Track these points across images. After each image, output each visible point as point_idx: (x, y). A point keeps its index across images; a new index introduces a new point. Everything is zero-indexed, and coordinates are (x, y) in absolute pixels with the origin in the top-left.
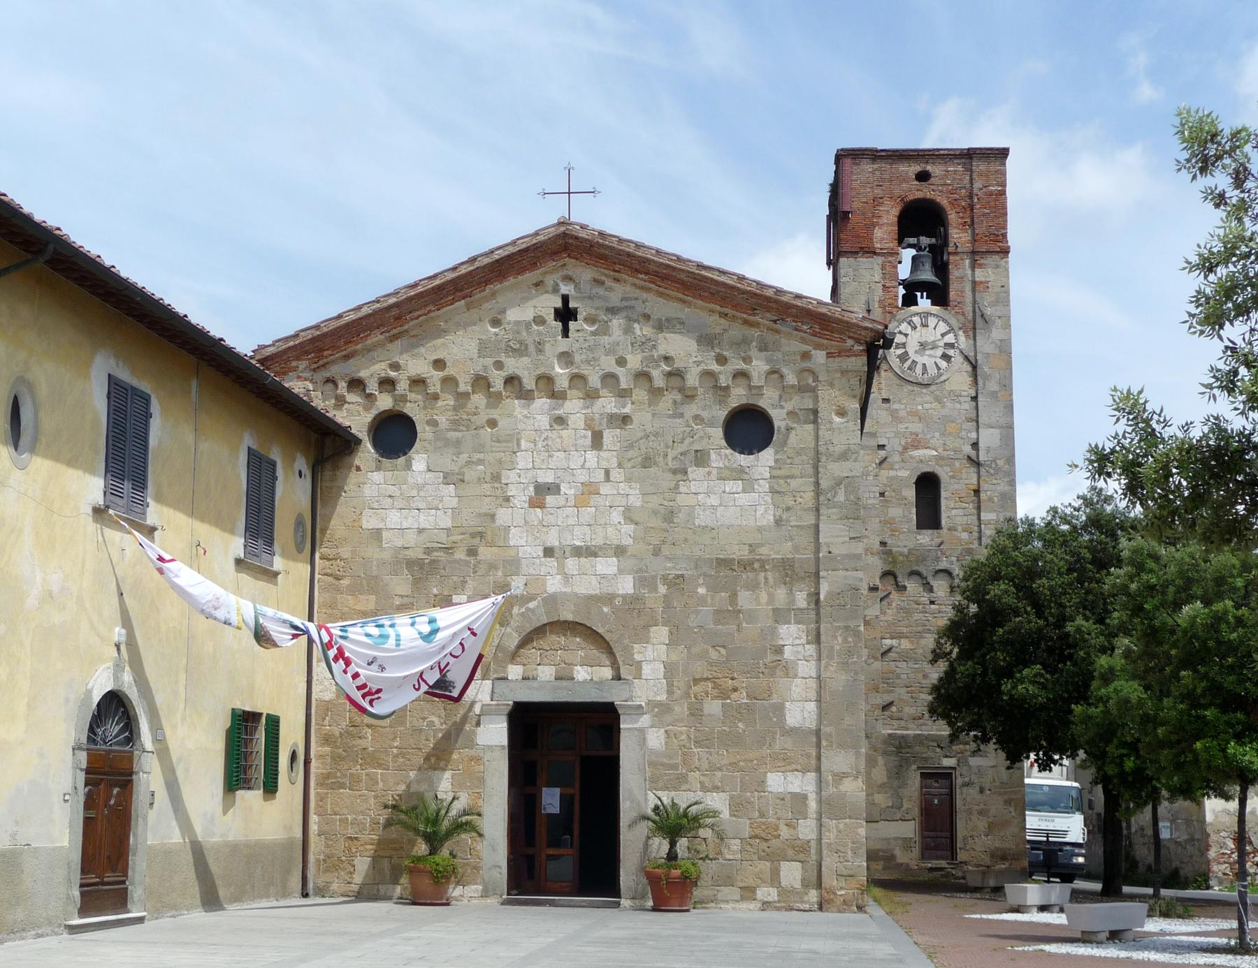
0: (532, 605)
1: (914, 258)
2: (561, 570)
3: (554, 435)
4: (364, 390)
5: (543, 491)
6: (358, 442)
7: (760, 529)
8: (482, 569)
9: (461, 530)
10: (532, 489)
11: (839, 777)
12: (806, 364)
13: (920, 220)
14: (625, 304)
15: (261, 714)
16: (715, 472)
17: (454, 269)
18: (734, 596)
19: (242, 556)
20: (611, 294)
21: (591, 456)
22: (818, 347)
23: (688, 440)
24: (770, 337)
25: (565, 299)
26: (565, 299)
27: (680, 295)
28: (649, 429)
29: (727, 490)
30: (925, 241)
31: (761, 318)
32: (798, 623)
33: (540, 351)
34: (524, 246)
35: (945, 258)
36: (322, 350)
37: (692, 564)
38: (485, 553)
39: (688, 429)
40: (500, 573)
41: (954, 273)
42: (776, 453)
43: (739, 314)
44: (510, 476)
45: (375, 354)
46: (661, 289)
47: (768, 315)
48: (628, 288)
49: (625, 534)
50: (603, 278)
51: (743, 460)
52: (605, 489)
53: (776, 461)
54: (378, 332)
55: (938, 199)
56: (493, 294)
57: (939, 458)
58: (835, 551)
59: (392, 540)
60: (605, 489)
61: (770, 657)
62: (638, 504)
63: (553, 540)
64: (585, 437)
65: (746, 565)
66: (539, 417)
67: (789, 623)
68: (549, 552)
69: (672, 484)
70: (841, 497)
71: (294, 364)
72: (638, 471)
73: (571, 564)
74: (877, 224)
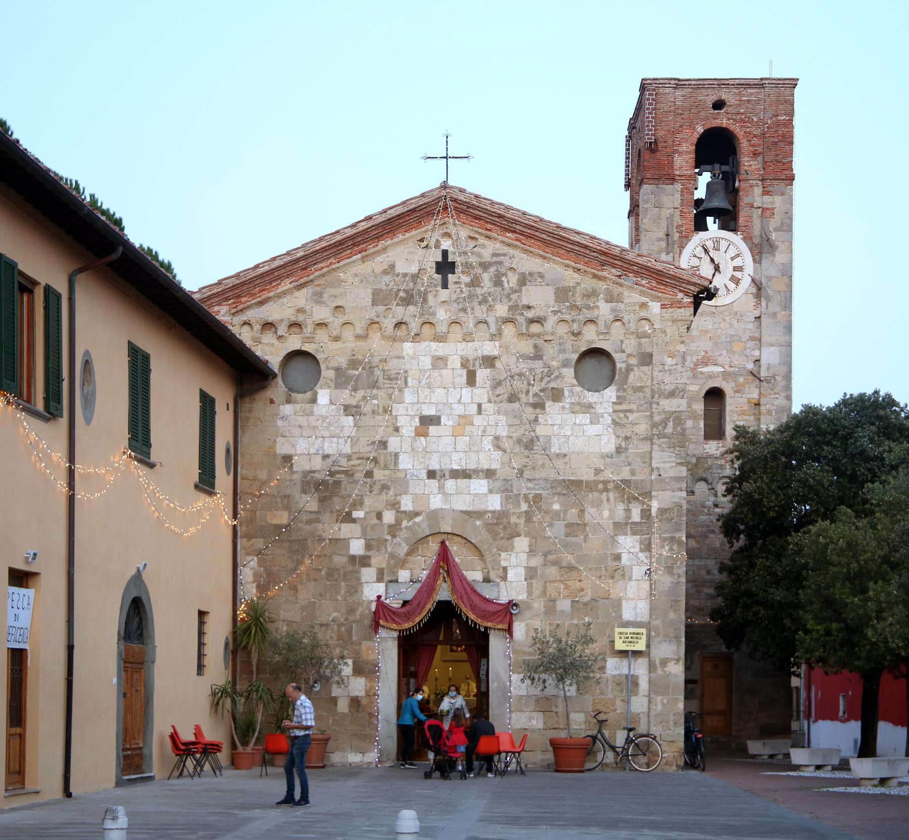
0: (418, 519)
5: (428, 421)
11: (664, 662)
13: (716, 149)
21: (466, 392)
22: (658, 299)
43: (589, 269)
44: (398, 409)
49: (491, 459)
53: (618, 397)
58: (664, 475)
59: (301, 465)
60: (478, 420)
61: (612, 564)
62: (505, 434)
70: (669, 430)
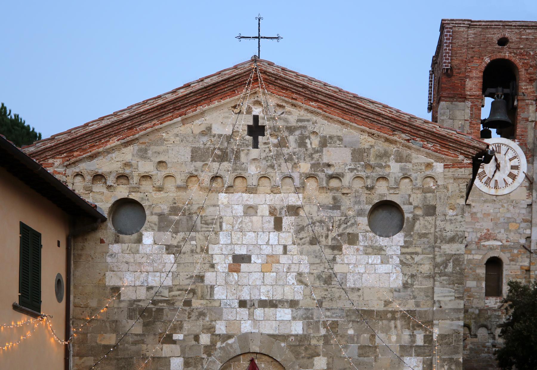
0: (230, 341)
1: (493, 103)
2: (251, 315)
3: (247, 219)
4: (105, 183)
5: (240, 260)
6: (104, 220)
7: (392, 291)
8: (194, 315)
9: (178, 287)
10: (230, 258)
12: (429, 172)
14: (300, 124)
15: (373, 311)
16: (361, 248)
17: (174, 92)
18: (373, 336)
19: (17, 302)
20: (289, 117)
21: (274, 237)
23: (344, 226)
24: (405, 152)
25: (256, 118)
26: (256, 118)
27: (340, 119)
28: (316, 218)
29: (370, 262)
30: (500, 91)
31: (400, 137)
32: (418, 355)
33: (237, 157)
34: (227, 76)
35: (516, 103)
36: (72, 151)
37: (344, 314)
38: (196, 303)
39: (343, 218)
40: (207, 319)
41: (522, 115)
42: (406, 236)
43: (382, 134)
44: (214, 249)
45: (114, 155)
46: (327, 114)
47: (403, 135)
48: (302, 112)
49: (293, 291)
50: (284, 104)
51: (382, 241)
52: (284, 259)
53: (405, 242)
54: (115, 139)
55: (513, 59)
56: (203, 113)
57: (503, 248)
59: (127, 295)
63: (245, 296)
64: (269, 222)
65: (381, 315)
66: (236, 207)
67: (411, 356)
68: (243, 304)
69: (331, 257)
70: (449, 269)
71: (51, 161)
72: (307, 247)
73: (259, 312)
74: (468, 77)
